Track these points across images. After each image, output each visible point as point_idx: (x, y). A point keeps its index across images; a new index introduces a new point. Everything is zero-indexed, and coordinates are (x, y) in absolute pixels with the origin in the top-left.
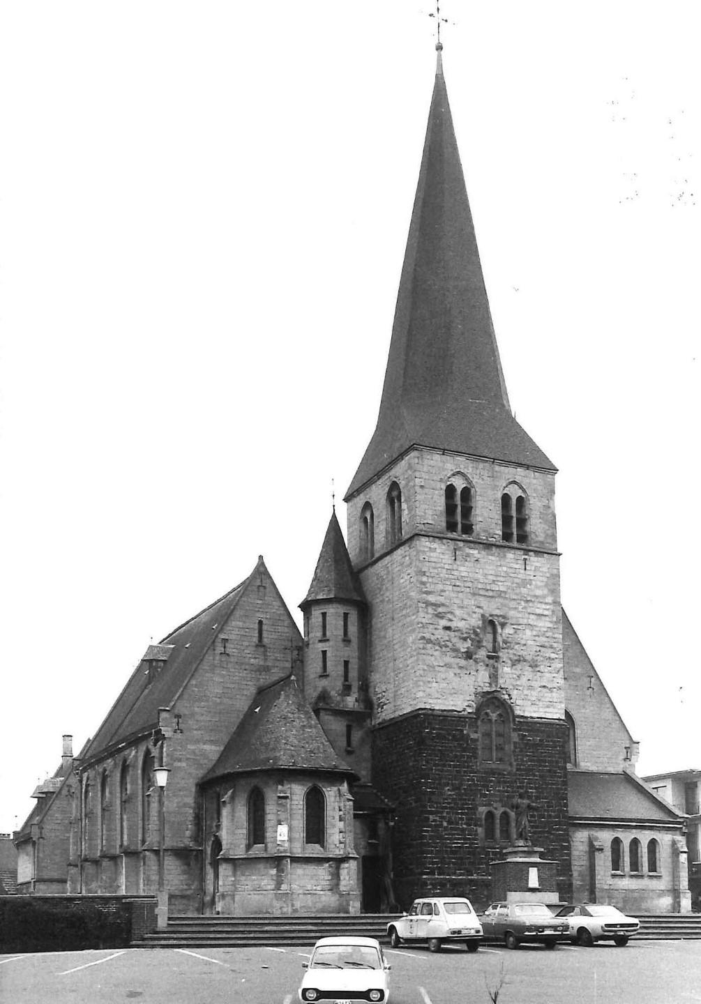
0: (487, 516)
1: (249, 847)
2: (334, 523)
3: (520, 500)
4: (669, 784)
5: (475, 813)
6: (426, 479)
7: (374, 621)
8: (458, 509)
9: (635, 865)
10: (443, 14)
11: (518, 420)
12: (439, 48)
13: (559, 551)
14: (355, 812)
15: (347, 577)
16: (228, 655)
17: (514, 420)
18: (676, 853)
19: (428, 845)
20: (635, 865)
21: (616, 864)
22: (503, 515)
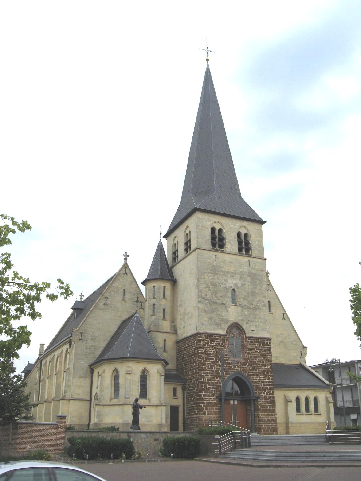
0: (231, 244)
1: (111, 399)
2: (160, 247)
3: (246, 235)
4: (254, 255)
5: (339, 411)
6: (201, 226)
7: (178, 290)
8: (217, 241)
9: (307, 410)
10: (209, 49)
11: (244, 199)
12: (207, 60)
13: (265, 257)
14: (345, 413)
15: (164, 269)
16: (108, 305)
17: (243, 199)
18: (328, 402)
19: (215, 399)
20: (307, 410)
21: (298, 410)
22: (238, 241)
